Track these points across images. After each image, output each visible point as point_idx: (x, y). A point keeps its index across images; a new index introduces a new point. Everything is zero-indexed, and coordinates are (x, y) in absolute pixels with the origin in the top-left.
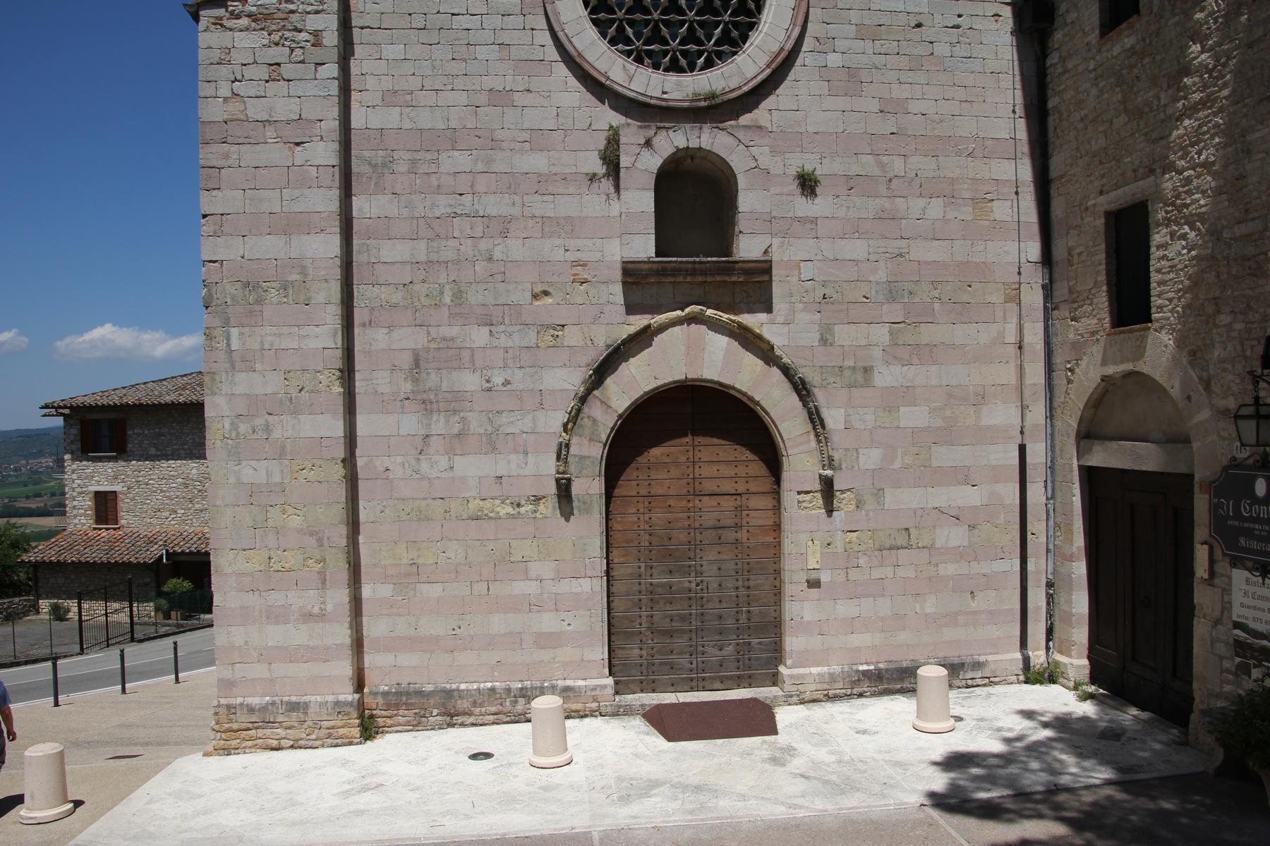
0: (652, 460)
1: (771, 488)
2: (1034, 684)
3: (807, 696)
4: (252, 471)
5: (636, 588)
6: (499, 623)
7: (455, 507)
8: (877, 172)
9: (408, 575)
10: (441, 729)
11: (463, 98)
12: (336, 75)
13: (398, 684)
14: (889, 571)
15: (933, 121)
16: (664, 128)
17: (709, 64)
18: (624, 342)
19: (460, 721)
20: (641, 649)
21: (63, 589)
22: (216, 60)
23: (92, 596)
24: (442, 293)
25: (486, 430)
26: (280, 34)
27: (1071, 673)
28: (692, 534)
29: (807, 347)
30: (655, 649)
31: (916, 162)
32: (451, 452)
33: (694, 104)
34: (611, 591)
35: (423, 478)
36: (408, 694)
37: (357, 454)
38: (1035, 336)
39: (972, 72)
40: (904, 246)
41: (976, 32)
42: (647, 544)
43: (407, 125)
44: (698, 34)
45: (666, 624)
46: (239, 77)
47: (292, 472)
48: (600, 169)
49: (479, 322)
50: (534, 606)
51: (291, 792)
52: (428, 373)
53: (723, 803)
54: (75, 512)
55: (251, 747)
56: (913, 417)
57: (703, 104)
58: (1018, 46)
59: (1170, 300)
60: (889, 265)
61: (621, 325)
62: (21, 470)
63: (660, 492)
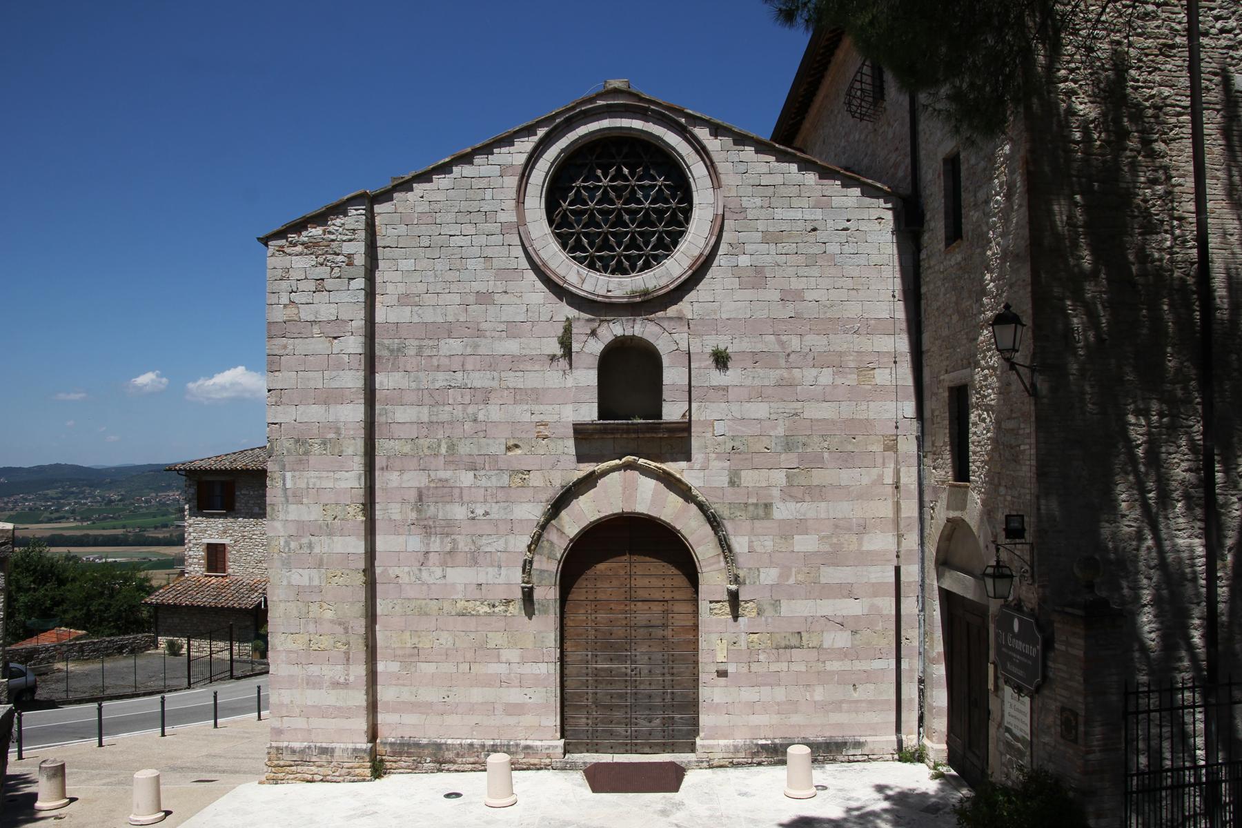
0: (598, 572)
2: (905, 762)
3: (715, 763)
4: (298, 577)
5: (584, 671)
6: (477, 695)
7: (447, 606)
8: (777, 348)
9: (412, 655)
10: (432, 772)
11: (457, 299)
12: (363, 287)
14: (784, 666)
15: (825, 306)
16: (606, 320)
17: (647, 266)
18: (575, 484)
19: (446, 768)
20: (588, 719)
21: (179, 628)
22: (279, 277)
23: (200, 636)
24: (439, 446)
27: (932, 755)
31: (810, 339)
32: (444, 564)
35: (423, 584)
36: (409, 745)
38: (909, 478)
39: (858, 266)
40: (799, 407)
41: (862, 233)
43: (416, 319)
45: (607, 701)
46: (295, 289)
47: (327, 577)
50: (503, 682)
52: (428, 506)
54: (190, 561)
56: (805, 543)
57: (638, 299)
62: (151, 502)
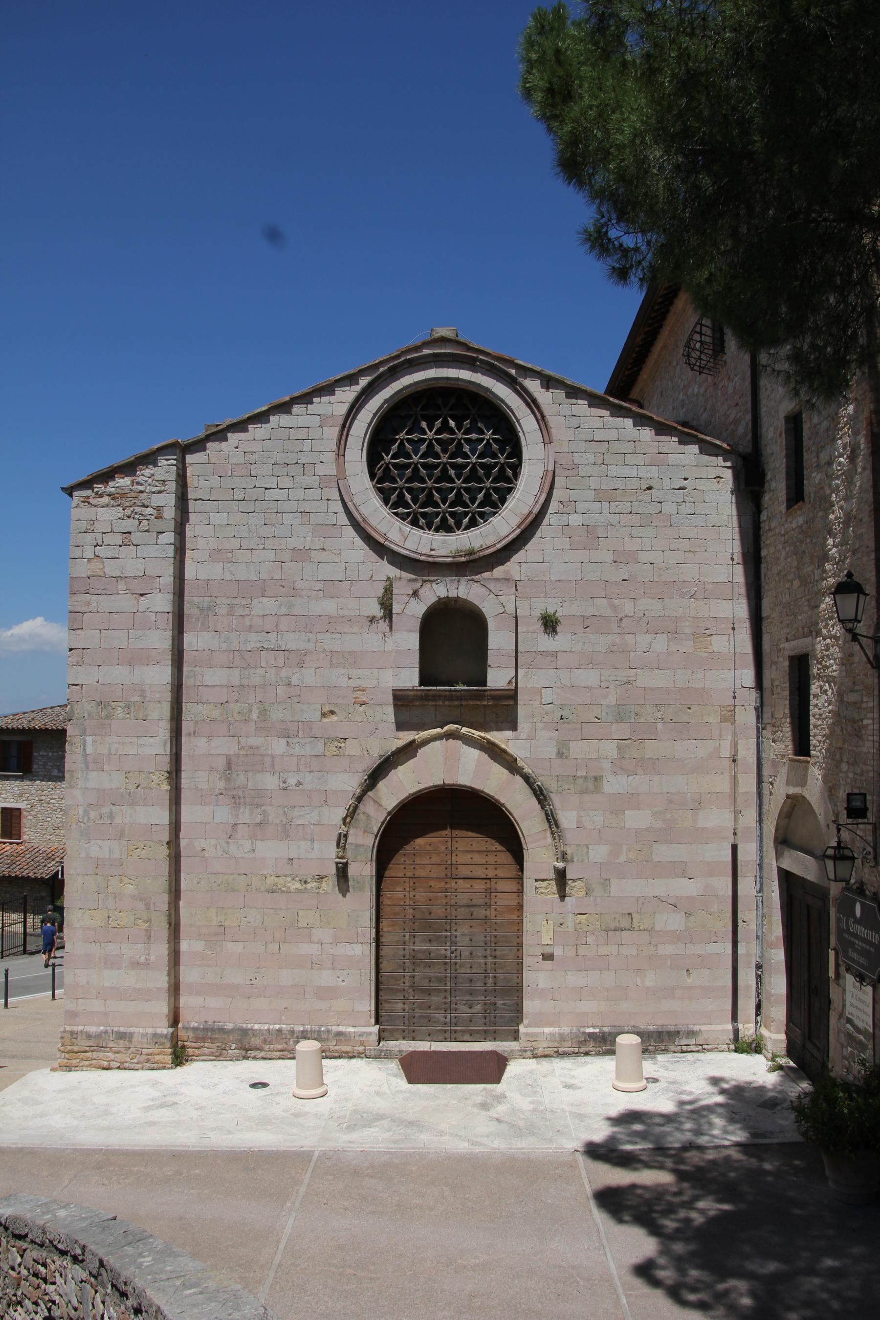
0: (417, 848)
1: (517, 874)
2: (742, 1053)
3: (540, 1052)
5: (401, 953)
8: (609, 612)
11: (272, 555)
12: (172, 541)
13: (205, 1022)
14: (613, 949)
15: (660, 569)
16: (429, 581)
17: (473, 523)
18: (394, 754)
19: (253, 1055)
20: (404, 1004)
22: (83, 530)
24: (250, 711)
25: (281, 821)
26: (132, 509)
27: (770, 1046)
28: (449, 910)
29: (545, 759)
30: (416, 1004)
32: (253, 838)
33: (456, 559)
34: (381, 954)
36: (213, 1030)
37: (181, 837)
38: (747, 751)
39: (695, 527)
41: (700, 492)
42: (411, 917)
43: (228, 577)
44: (464, 498)
45: (425, 984)
46: (100, 543)
48: (378, 612)
49: (279, 734)
50: (315, 964)
51: (107, 1105)
52: (238, 775)
53: (423, 1137)
55: (87, 1066)
56: (637, 819)
57: (463, 559)
58: (737, 503)
59: (819, 742)
60: (618, 691)
61: (392, 739)
63: (423, 874)
